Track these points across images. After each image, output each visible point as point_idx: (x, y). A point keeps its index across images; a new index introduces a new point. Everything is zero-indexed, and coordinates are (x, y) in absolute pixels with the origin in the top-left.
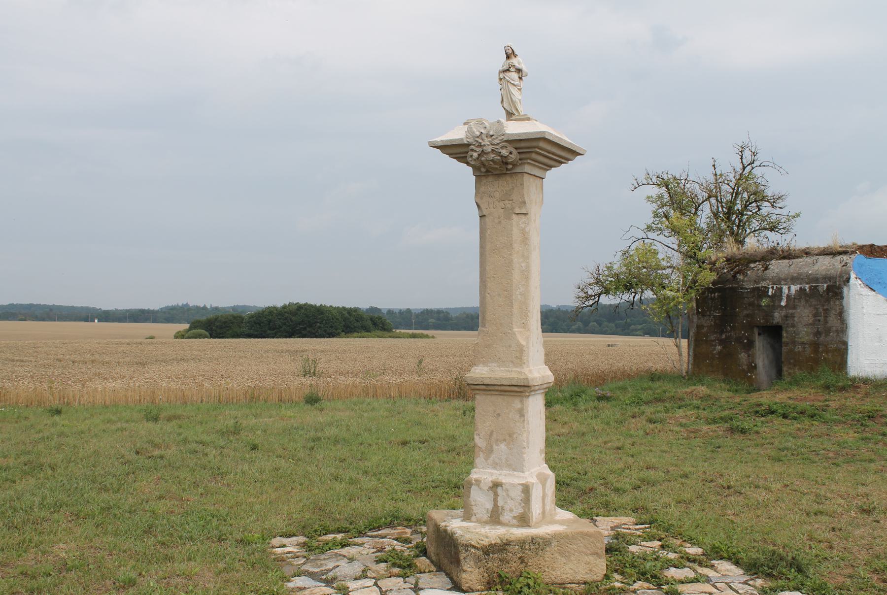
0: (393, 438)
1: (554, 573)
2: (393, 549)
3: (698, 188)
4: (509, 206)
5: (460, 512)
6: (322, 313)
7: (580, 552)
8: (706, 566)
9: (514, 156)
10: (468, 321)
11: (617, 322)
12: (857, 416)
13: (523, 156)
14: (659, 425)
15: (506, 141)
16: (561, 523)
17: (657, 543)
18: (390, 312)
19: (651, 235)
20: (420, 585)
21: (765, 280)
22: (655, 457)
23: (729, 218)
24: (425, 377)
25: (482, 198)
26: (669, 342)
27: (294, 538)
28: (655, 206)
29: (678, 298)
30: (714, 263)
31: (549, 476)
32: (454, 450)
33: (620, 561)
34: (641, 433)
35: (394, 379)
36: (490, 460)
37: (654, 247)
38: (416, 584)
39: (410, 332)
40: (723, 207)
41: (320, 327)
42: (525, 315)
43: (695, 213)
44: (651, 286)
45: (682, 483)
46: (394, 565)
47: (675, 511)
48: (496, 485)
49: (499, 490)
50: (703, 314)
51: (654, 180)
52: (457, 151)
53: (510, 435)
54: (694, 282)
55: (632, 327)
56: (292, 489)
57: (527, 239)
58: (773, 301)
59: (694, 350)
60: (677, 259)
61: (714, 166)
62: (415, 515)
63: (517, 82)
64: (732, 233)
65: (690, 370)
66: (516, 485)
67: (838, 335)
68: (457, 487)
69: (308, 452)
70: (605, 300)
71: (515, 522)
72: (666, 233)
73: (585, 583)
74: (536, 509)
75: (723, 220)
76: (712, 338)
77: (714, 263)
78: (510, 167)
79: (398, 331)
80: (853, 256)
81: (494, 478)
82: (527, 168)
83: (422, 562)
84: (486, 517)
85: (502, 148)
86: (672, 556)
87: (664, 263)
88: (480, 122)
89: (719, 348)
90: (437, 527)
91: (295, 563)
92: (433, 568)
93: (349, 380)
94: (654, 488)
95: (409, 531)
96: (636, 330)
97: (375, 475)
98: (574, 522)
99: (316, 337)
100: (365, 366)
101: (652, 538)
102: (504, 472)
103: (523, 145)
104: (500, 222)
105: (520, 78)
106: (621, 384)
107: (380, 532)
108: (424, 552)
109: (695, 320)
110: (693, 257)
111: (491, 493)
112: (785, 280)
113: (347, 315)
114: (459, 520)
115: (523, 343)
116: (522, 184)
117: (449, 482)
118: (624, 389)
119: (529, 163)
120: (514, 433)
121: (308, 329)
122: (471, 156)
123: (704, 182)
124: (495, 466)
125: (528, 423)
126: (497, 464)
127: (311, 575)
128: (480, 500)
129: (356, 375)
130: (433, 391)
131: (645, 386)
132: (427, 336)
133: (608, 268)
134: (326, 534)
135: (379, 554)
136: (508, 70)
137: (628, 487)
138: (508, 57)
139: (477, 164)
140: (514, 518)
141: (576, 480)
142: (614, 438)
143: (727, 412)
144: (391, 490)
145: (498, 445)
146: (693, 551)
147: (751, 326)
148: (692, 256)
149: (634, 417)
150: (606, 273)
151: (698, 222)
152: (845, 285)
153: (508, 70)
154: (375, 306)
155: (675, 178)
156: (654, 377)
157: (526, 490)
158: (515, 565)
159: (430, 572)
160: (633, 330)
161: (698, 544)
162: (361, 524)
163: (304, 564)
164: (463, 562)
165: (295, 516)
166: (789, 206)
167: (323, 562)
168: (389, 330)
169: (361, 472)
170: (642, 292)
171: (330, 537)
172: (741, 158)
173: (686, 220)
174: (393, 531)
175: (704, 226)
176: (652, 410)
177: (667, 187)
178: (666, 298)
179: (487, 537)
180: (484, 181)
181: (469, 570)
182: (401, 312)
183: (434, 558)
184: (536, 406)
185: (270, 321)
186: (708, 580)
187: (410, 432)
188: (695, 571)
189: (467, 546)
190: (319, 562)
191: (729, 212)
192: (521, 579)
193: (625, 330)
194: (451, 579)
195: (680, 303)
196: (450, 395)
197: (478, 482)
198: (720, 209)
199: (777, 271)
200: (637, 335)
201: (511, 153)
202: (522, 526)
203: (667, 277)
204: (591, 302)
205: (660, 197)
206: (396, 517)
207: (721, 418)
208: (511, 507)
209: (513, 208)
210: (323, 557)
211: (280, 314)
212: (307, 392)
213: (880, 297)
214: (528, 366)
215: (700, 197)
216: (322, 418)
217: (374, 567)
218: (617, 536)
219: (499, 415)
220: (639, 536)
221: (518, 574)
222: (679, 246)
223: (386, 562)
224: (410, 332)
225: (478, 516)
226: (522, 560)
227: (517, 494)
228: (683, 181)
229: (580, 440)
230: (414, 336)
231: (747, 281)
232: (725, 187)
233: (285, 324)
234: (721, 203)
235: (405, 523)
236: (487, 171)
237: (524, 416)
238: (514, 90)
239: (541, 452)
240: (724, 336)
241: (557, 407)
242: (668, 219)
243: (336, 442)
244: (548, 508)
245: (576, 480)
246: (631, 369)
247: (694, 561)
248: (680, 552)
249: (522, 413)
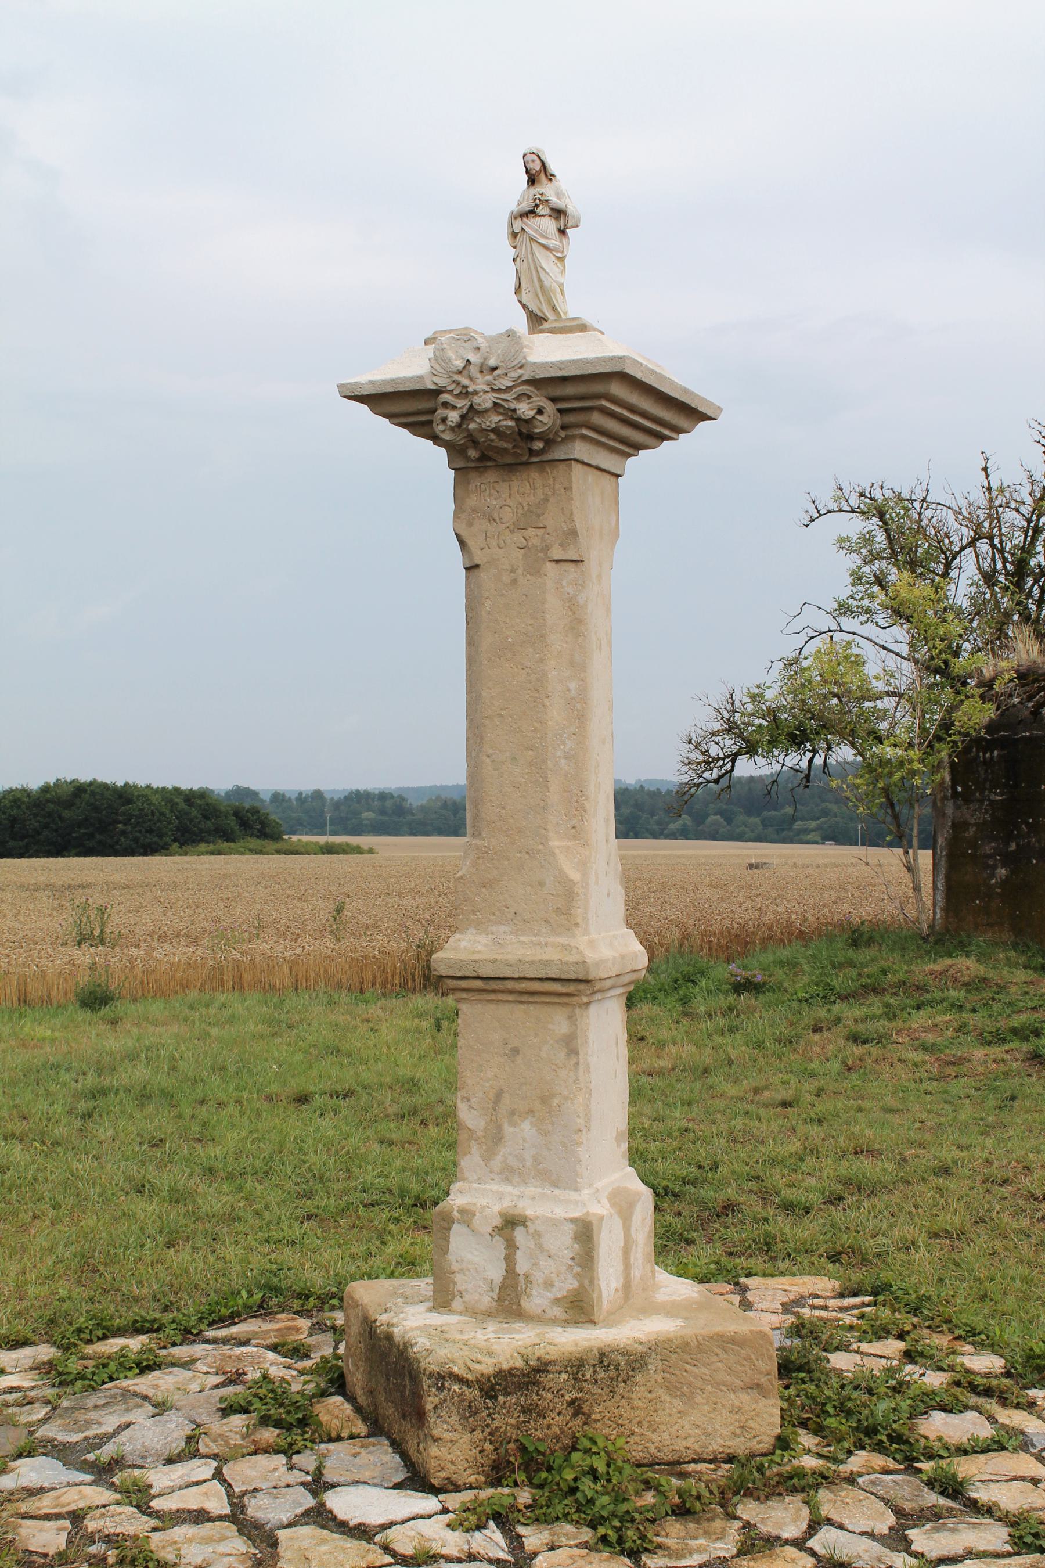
0: (274, 1088)
1: (655, 1437)
2: (265, 1377)
3: (951, 517)
4: (535, 541)
5: (424, 1285)
6: (129, 801)
7: (717, 1384)
8: (1018, 1406)
9: (548, 420)
10: (445, 817)
11: (765, 814)
13: (571, 419)
14: (875, 1050)
15: (528, 382)
16: (670, 1310)
17: (894, 1347)
18: (278, 798)
19: (847, 623)
20: (329, 1476)
22: (870, 1125)
23: (1019, 585)
24: (349, 942)
25: (470, 524)
26: (891, 858)
27: (27, 1351)
28: (854, 560)
29: (911, 762)
30: (990, 684)
31: (638, 1194)
32: (414, 1112)
33: (813, 1398)
34: (836, 1066)
35: (280, 948)
36: (497, 1163)
37: (855, 651)
38: (319, 1473)
39: (322, 840)
40: (1005, 561)
41: (123, 833)
42: (577, 805)
43: (945, 575)
44: (850, 736)
45: (939, 1189)
46: (265, 1421)
47: (924, 1259)
48: (511, 1223)
50: (966, 798)
51: (854, 501)
52: (408, 407)
53: (544, 1100)
54: (946, 725)
55: (799, 824)
56: (35, 1217)
57: (580, 621)
59: (948, 878)
60: (906, 673)
61: (985, 469)
62: (318, 1281)
63: (554, 242)
64: (1026, 618)
65: (939, 922)
66: (559, 1229)
68: (420, 1203)
69: (79, 1124)
70: (745, 768)
71: (557, 1312)
72: (880, 618)
73: (730, 1459)
74: (609, 1278)
75: (1006, 589)
76: (988, 849)
77: (990, 684)
78: (539, 445)
79: (295, 838)
81: (506, 1203)
82: (580, 450)
83: (335, 1410)
84: (487, 1301)
85: (518, 398)
86: (935, 1380)
87: (879, 686)
88: (465, 336)
89: (1002, 872)
90: (369, 1327)
91: (23, 1419)
92: (361, 1428)
93: (179, 953)
94: (874, 1200)
95: (304, 1323)
96: (807, 831)
97: (230, 1177)
98: (701, 1306)
99: (116, 854)
100: (216, 920)
101: (881, 1332)
102: (531, 1190)
103: (570, 390)
104: (514, 582)
105: (562, 232)
106: (784, 953)
107: (234, 1329)
108: (339, 1384)
109: (949, 811)
110: (944, 671)
111: (499, 1243)
113: (183, 805)
114: (422, 1308)
115: (575, 875)
116: (568, 489)
117: (403, 1193)
118: (791, 964)
119: (584, 437)
120: (552, 1095)
121: (98, 837)
122: (444, 420)
123: (964, 504)
124: (509, 1174)
125: (587, 1070)
126: (512, 1171)
127: (60, 1451)
128: (473, 1258)
129: (196, 941)
130: (368, 975)
131: (840, 957)
132: (358, 850)
133: (753, 697)
134: (105, 1337)
135: (230, 1390)
136: (532, 212)
137: (815, 1198)
138: (532, 180)
139: (459, 439)
140: (557, 1301)
141: (694, 1182)
142: (776, 1080)
143: (1024, 1017)
144: (267, 1215)
145: (513, 1124)
146: (984, 1363)
148: (939, 668)
149: (817, 1029)
150: (750, 708)
151: (951, 593)
153: (532, 212)
154: (244, 784)
155: (899, 498)
156: (859, 937)
157: (585, 1233)
158: (558, 1421)
159: (352, 1437)
160: (800, 832)
161: (991, 1346)
162: (190, 1307)
163: (45, 1420)
164: (432, 1418)
165: (31, 1290)
167: (93, 1415)
168: (276, 837)
169: (198, 1170)
170: (829, 748)
171: (113, 1345)
173: (924, 588)
174: (267, 1326)
175: (965, 604)
176: (858, 1012)
177: (881, 516)
178: (884, 763)
179: (490, 1354)
180: (476, 481)
181: (447, 1436)
182: (301, 798)
183: (362, 1400)
184: (605, 1025)
185: (14, 820)
186: (1025, 1445)
187: (315, 1072)
188: (991, 1419)
189: (443, 1378)
190: (81, 1416)
191: (1020, 570)
192: (576, 1456)
193: (784, 831)
194: (404, 1456)
195: (913, 773)
196: (405, 982)
197: (467, 1215)
198: (999, 565)
200: (808, 842)
201: (540, 411)
202: (576, 1323)
203: (882, 715)
204: (716, 773)
205: (867, 540)
206: (277, 1290)
207: (1014, 1031)
208: (549, 1273)
209: (546, 549)
210: (92, 1400)
211: (35, 805)
212: (84, 980)
214: (586, 932)
215: (955, 538)
216: (114, 1042)
217: (218, 1426)
218: (798, 1330)
219: (516, 1051)
220: (851, 1328)
221: (568, 1442)
222: (911, 645)
223: (246, 1411)
224: (322, 840)
225: (467, 1297)
226: (576, 1408)
227: (562, 1244)
228: (917, 505)
229: (698, 1085)
230: (329, 850)
232: (1010, 516)
233: (46, 826)
234: (1002, 551)
235: (296, 1304)
236: (483, 457)
237: (576, 1053)
238: (546, 261)
239: (618, 1139)
240: (1013, 846)
241: (645, 1009)
242: (883, 587)
243: (144, 1096)
244: (636, 1274)
245: (694, 1182)
246: (805, 920)
247: (988, 1392)
248: (952, 1368)
249: (571, 1046)
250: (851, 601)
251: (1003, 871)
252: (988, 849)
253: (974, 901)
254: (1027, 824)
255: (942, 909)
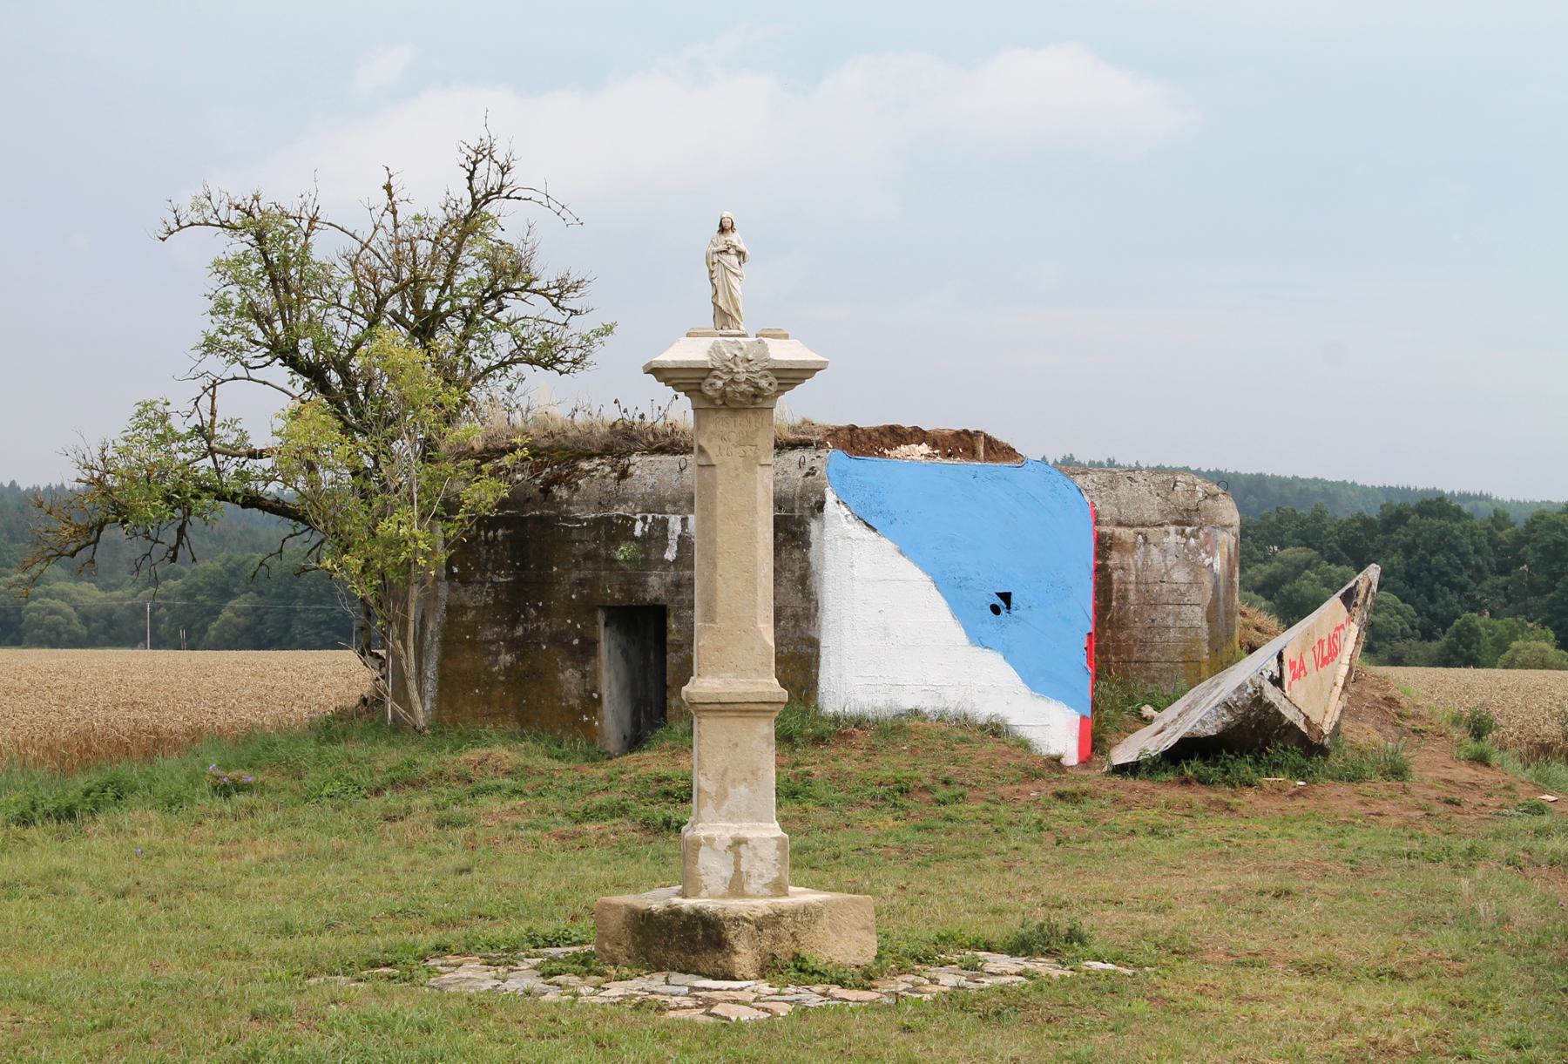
12: (883, 789)
21: (626, 501)
48: (738, 842)
49: (743, 849)
50: (465, 580)
58: (646, 551)
61: (388, 187)
67: (796, 625)
80: (822, 452)
81: (732, 833)
84: (722, 889)
89: (506, 658)
102: (745, 825)
111: (730, 855)
112: (674, 502)
124: (731, 816)
126: (733, 814)
138: (722, 230)
140: (766, 885)
147: (588, 608)
152: (813, 516)
166: (595, 305)
172: (470, 178)
177: (260, 237)
197: (710, 841)
199: (651, 480)
207: (601, 808)
209: (757, 458)
213: (886, 544)
231: (582, 500)
240: (519, 631)
250: (220, 335)
251: (508, 658)
252: (489, 634)
253: (472, 690)
254: (536, 608)
255: (432, 700)
